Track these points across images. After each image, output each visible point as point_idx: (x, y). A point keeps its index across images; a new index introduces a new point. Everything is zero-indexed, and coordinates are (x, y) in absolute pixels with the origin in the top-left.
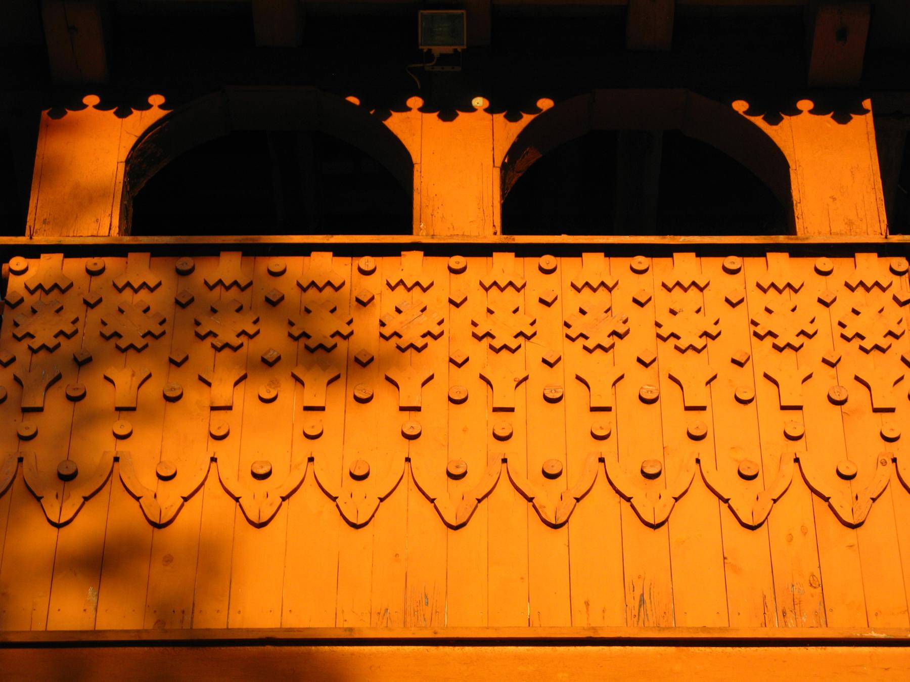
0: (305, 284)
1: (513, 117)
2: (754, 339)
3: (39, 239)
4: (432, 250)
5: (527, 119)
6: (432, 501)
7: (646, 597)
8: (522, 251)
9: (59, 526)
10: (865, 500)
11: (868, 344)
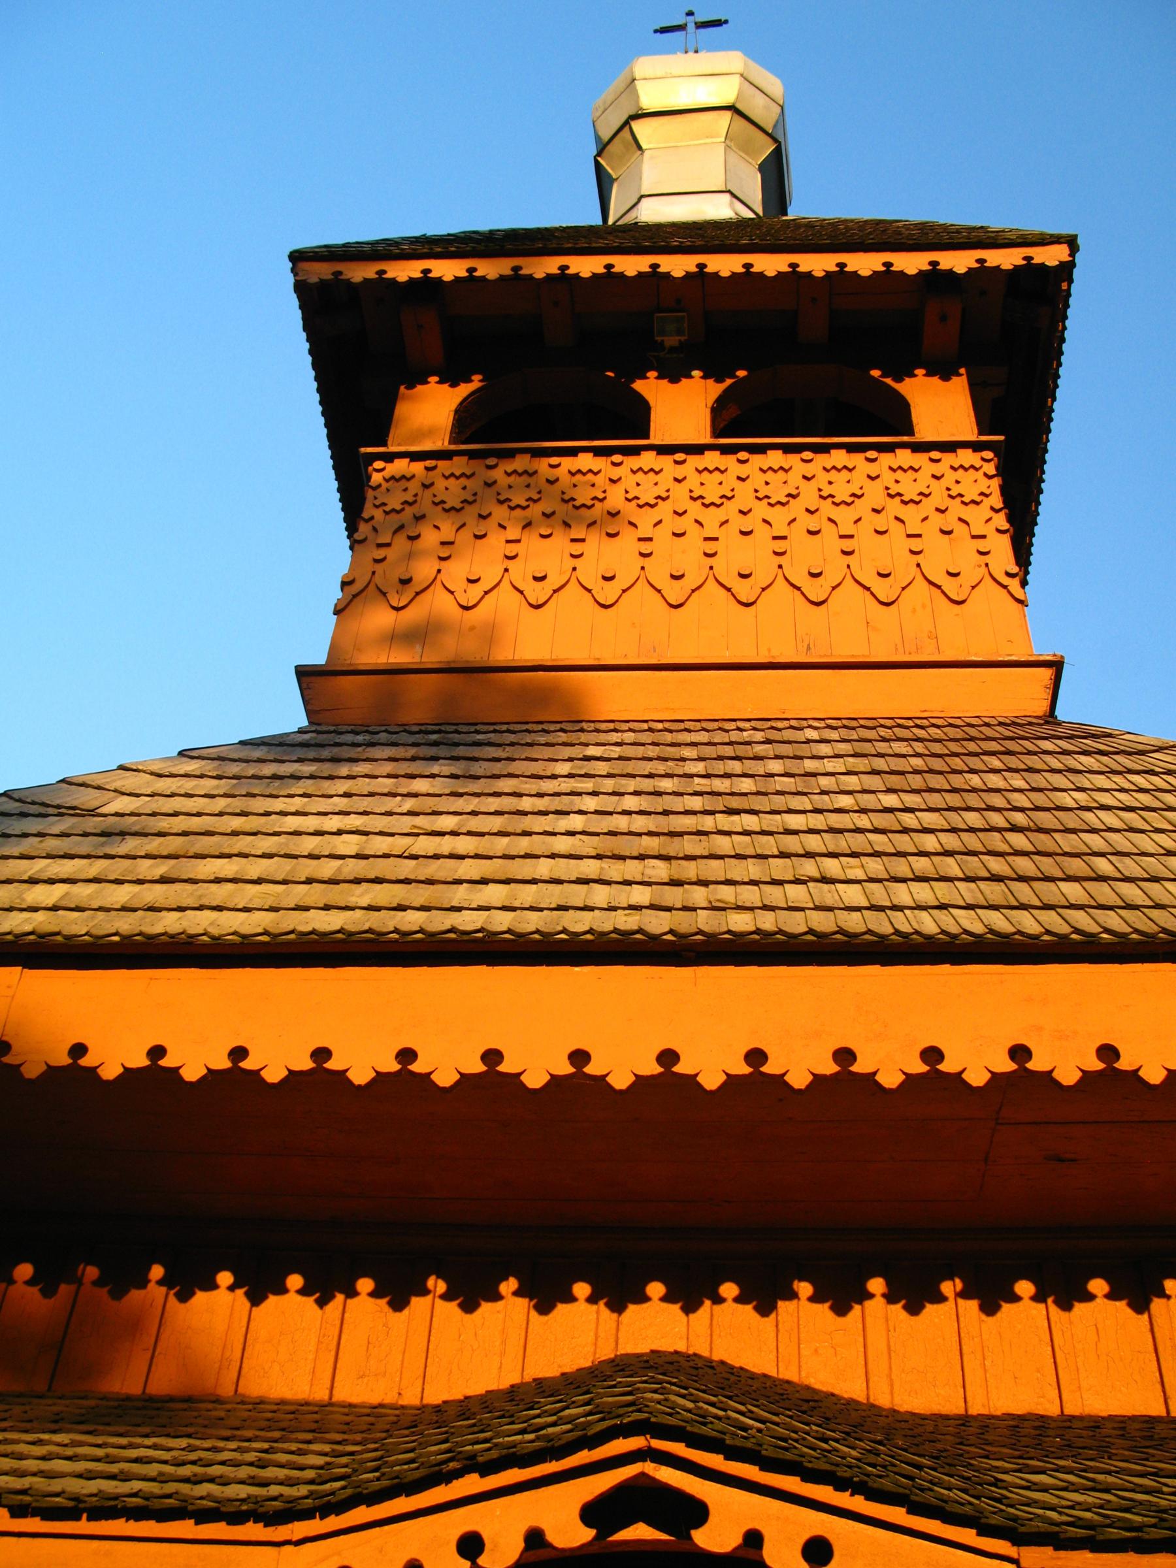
0: (573, 471)
1: (719, 380)
2: (888, 499)
3: (393, 448)
4: (664, 450)
5: (729, 382)
6: (659, 591)
7: (812, 646)
8: (726, 450)
9: (397, 609)
10: (967, 589)
11: (966, 500)
